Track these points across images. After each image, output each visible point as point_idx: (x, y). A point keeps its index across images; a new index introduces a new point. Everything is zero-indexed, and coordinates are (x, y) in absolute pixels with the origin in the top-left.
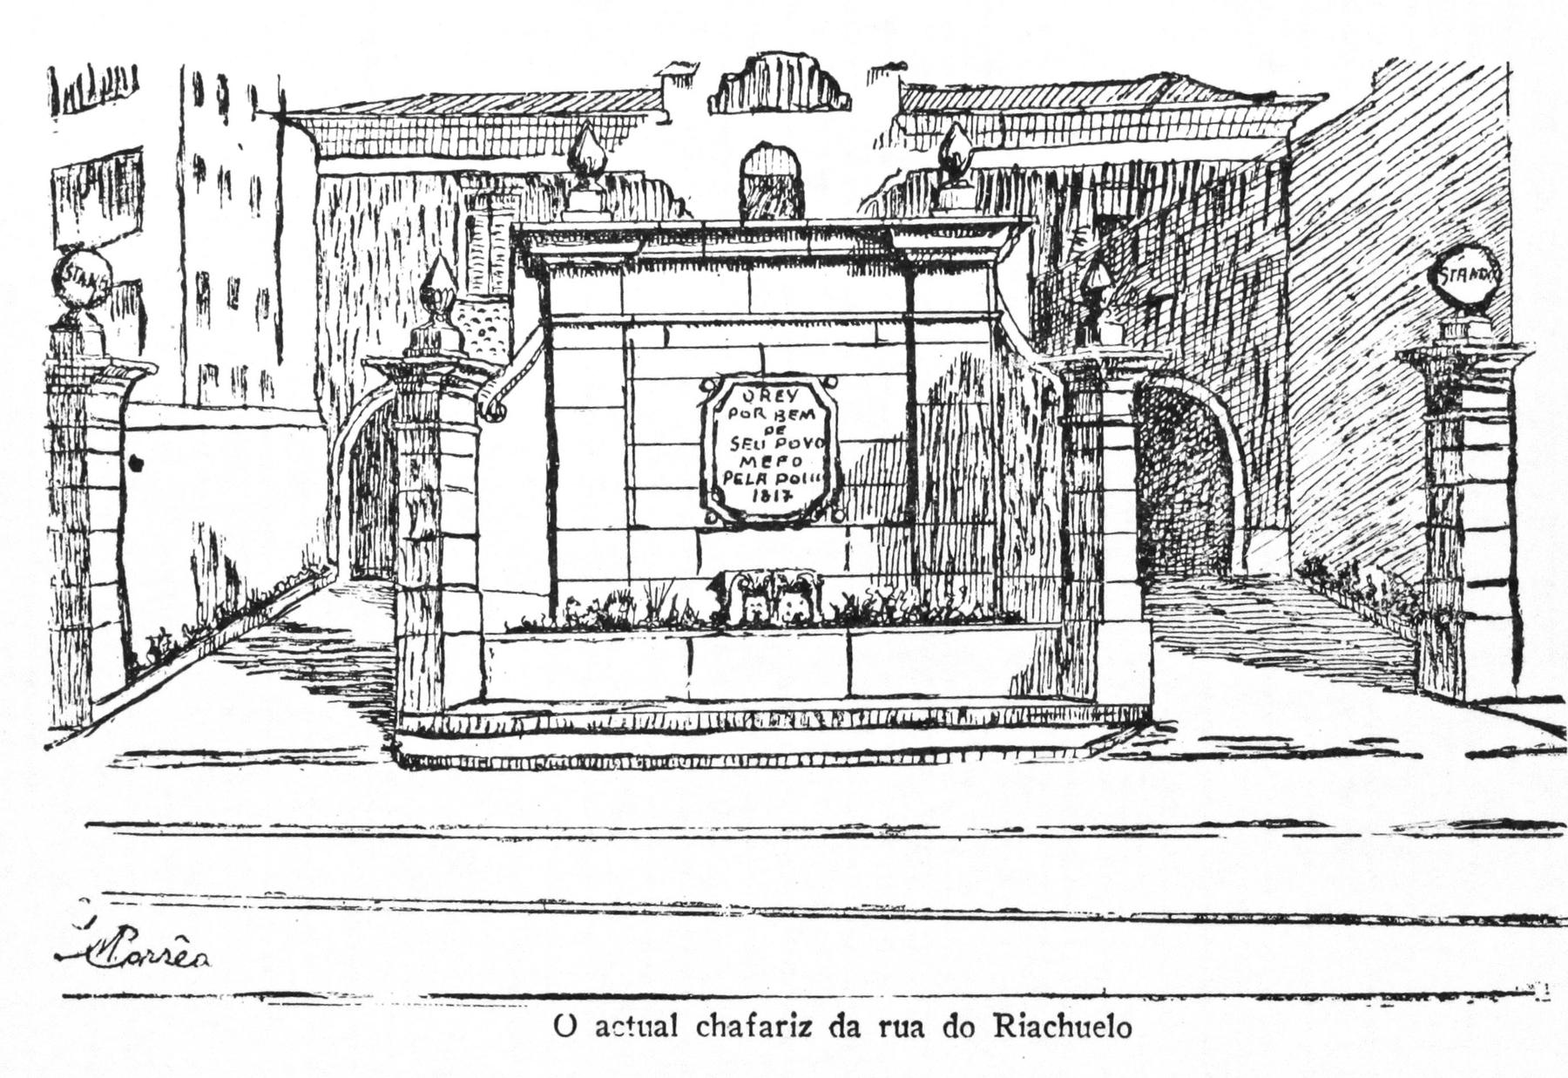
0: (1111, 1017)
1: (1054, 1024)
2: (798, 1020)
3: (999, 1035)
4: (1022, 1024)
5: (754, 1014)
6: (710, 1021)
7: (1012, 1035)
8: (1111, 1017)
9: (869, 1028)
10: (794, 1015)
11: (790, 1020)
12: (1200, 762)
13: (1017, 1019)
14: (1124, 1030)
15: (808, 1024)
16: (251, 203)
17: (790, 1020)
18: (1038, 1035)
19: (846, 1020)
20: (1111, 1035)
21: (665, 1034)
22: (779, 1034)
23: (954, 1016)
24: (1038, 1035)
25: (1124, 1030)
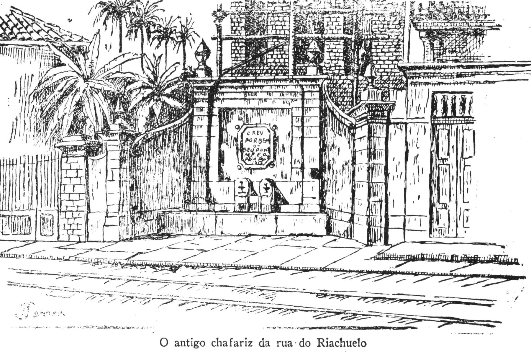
0: (359, 339)
1: (338, 342)
2: (248, 341)
3: (319, 346)
4: (327, 342)
5: (232, 339)
6: (340, 341)
7: (188, 346)
8: (359, 339)
9: (273, 344)
10: (246, 339)
11: (245, 340)
12: (471, 306)
13: (326, 340)
14: (308, 344)
15: (251, 342)
16: (489, 306)
17: (245, 340)
18: (333, 346)
19: (265, 341)
20: (359, 346)
21: (238, 346)
22: (241, 346)
23: (303, 339)
24: (333, 346)
25: (308, 344)
